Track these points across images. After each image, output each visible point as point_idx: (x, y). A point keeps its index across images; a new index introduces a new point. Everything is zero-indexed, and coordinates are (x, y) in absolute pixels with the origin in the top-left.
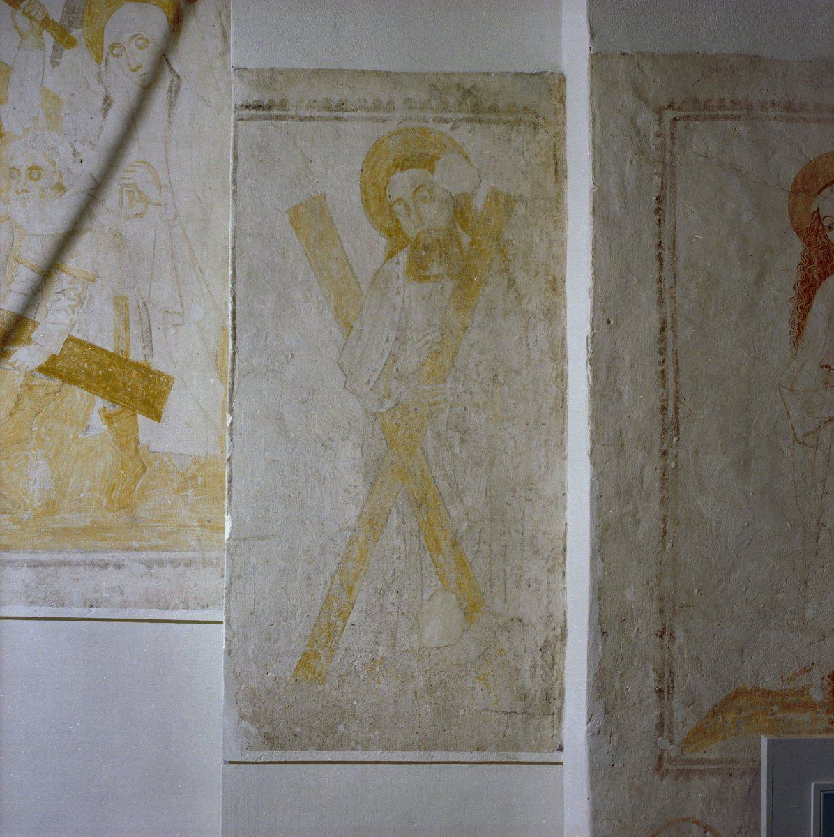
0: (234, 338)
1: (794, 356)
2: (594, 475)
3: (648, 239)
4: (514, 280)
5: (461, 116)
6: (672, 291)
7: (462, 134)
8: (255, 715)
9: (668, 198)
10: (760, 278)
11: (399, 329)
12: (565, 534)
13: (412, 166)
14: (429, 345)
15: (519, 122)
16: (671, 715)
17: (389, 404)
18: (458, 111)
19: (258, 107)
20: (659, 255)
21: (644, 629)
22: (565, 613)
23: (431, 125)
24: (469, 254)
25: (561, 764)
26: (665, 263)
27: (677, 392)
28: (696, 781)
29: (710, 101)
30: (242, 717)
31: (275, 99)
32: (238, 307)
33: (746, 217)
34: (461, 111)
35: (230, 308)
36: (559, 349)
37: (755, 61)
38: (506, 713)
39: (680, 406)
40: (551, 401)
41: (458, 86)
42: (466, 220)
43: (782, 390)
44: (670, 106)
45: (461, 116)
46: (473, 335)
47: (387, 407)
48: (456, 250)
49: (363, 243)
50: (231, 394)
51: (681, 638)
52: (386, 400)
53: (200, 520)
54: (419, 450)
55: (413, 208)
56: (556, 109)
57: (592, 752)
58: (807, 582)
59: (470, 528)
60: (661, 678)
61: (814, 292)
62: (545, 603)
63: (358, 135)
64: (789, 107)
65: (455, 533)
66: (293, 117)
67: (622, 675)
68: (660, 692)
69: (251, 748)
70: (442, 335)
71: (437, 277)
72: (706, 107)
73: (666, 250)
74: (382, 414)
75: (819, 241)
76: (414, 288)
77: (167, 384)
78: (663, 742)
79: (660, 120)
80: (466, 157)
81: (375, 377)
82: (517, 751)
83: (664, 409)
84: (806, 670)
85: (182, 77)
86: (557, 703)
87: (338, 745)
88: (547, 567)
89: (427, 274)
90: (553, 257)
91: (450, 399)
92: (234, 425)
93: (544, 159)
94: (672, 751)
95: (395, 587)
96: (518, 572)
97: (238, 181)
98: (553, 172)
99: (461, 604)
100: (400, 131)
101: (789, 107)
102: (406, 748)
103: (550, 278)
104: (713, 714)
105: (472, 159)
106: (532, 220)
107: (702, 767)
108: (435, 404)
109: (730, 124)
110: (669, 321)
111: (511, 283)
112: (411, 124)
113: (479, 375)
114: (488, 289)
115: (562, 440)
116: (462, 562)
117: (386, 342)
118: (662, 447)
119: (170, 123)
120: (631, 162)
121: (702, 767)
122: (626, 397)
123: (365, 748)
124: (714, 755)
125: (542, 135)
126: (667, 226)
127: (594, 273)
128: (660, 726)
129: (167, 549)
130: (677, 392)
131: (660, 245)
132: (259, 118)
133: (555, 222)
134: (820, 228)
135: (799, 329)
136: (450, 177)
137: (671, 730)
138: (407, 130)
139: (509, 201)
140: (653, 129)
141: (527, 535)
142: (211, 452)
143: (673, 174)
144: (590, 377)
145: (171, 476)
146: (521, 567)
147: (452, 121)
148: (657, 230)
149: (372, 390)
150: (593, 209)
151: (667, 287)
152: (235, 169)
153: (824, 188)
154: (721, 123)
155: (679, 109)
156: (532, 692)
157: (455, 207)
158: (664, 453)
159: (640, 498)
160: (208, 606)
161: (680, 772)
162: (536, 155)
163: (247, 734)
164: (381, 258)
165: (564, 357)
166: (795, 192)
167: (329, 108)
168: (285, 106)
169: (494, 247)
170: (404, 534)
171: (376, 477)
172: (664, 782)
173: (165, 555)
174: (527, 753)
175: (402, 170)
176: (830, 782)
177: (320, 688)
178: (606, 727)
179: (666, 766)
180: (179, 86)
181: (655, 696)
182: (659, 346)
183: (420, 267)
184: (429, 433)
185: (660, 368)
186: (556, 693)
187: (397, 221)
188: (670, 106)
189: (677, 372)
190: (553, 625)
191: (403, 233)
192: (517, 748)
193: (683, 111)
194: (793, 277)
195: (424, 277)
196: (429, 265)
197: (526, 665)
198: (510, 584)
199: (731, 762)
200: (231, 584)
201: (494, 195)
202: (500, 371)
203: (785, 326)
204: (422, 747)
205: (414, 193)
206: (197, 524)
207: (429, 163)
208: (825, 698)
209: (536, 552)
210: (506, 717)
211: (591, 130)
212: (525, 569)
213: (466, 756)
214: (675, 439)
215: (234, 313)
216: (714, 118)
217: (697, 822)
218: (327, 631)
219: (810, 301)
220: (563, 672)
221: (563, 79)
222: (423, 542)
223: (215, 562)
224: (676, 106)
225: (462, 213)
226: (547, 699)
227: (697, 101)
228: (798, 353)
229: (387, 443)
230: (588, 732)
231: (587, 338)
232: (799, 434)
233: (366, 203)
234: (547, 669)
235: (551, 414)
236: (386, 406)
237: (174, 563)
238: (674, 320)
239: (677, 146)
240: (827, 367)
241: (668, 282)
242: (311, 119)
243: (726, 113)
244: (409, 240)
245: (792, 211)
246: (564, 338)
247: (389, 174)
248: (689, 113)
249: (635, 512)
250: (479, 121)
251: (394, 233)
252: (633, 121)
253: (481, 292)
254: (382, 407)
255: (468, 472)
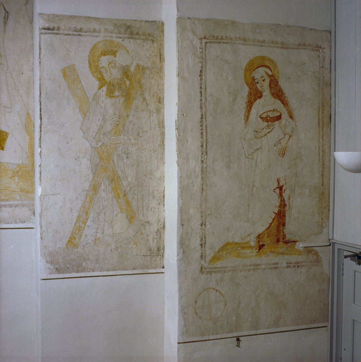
0: (41, 119)
1: (245, 128)
2: (179, 170)
3: (197, 86)
4: (145, 98)
5: (126, 36)
6: (205, 104)
7: (126, 43)
8: (52, 261)
9: (204, 71)
10: (235, 99)
11: (104, 116)
12: (164, 191)
13: (108, 54)
14: (114, 122)
15: (147, 39)
16: (205, 253)
17: (100, 144)
18: (125, 34)
19: (49, 29)
20: (201, 91)
21: (196, 223)
22: (164, 219)
23: (115, 39)
24: (131, 87)
25: (164, 273)
26: (203, 94)
27: (207, 140)
28: (213, 275)
29: (218, 36)
30: (47, 262)
31: (55, 26)
32: (42, 107)
33: (230, 78)
34: (125, 34)
35: (39, 108)
36: (162, 124)
37: (233, 23)
38: (144, 256)
39: (208, 145)
40: (159, 143)
41: (125, 25)
42: (128, 75)
43: (241, 139)
44: (205, 38)
45: (126, 36)
46: (131, 118)
47: (99, 145)
48: (124, 86)
49: (90, 83)
50: (40, 140)
51: (208, 226)
52: (99, 143)
53: (20, 189)
54: (111, 161)
55: (108, 70)
56: (160, 35)
57: (179, 267)
58: (249, 205)
59: (130, 189)
60: (201, 240)
61: (252, 105)
62: (157, 215)
63: (88, 42)
64: (245, 40)
65: (125, 191)
66: (62, 34)
67: (189, 239)
68: (201, 245)
69: (51, 273)
70: (119, 118)
71: (117, 96)
72: (217, 39)
73: (203, 89)
74: (97, 148)
75: (254, 87)
76: (109, 101)
77: (6, 136)
78: (203, 262)
79: (201, 43)
80: (128, 52)
81: (95, 134)
82: (148, 269)
83: (202, 146)
84: (249, 235)
85: (9, 12)
86: (162, 251)
87: (83, 270)
88: (158, 203)
89: (114, 95)
90: (159, 90)
91: (123, 142)
92: (42, 152)
93: (156, 54)
94: (206, 265)
95: (103, 212)
96: (148, 205)
97: (41, 58)
98: (159, 58)
99: (127, 217)
100: (103, 41)
101: (245, 40)
102: (108, 270)
103: (158, 98)
104: (219, 251)
105: (130, 52)
106: (152, 76)
107: (215, 270)
108: (117, 144)
109: (225, 45)
110: (204, 114)
111: (144, 99)
112: (107, 38)
113: (133, 133)
114: (136, 101)
115: (163, 157)
116: (128, 202)
117: (99, 120)
118: (201, 159)
119: (4, 31)
120: (191, 57)
121: (215, 270)
122: (189, 142)
123: (93, 271)
124: (220, 266)
125: (155, 44)
126: (204, 81)
127: (178, 97)
128: (202, 256)
129: (7, 200)
130: (207, 140)
131: (201, 88)
132: (49, 33)
133: (160, 77)
134: (254, 83)
135: (247, 118)
136: (121, 59)
137: (205, 258)
138: (106, 41)
139: (143, 68)
140: (199, 45)
141: (150, 192)
142: (24, 162)
143: (206, 62)
144: (177, 135)
145: (8, 172)
146: (149, 203)
147: (122, 38)
148: (200, 83)
149: (94, 139)
150: (178, 74)
151: (203, 102)
152: (40, 53)
153: (255, 69)
154: (222, 44)
155: (208, 39)
156: (153, 248)
157: (124, 70)
158: (202, 161)
159: (194, 177)
160: (24, 222)
161: (208, 272)
162: (153, 52)
163: (49, 268)
164: (96, 89)
165: (163, 126)
166: (246, 70)
167: (76, 31)
168: (59, 29)
169: (138, 86)
170: (106, 192)
171: (96, 171)
172: (203, 276)
173: (7, 203)
174: (151, 270)
175: (104, 56)
176: (288, 265)
177: (76, 250)
178: (183, 258)
179: (204, 270)
180: (8, 16)
181: (200, 246)
182: (201, 124)
183: (111, 92)
184: (115, 155)
185: (201, 132)
186: (162, 248)
187: (102, 75)
188: (205, 38)
189: (206, 132)
190: (160, 223)
191: (105, 80)
192: (148, 268)
193: (209, 40)
194: (246, 100)
195: (113, 97)
196: (114, 92)
197: (151, 238)
198: (145, 209)
199: (225, 268)
200: (42, 212)
201: (138, 66)
202: (140, 131)
203: (243, 117)
204: (114, 270)
205: (108, 65)
206: (19, 190)
207: (114, 53)
208: (255, 245)
209: (154, 197)
210: (144, 257)
211: (177, 45)
212: (150, 204)
213: (130, 272)
214: (206, 156)
215: (40, 109)
216: (219, 43)
217: (214, 289)
218: (79, 228)
219: (251, 108)
220: (164, 240)
221: (163, 24)
222: (113, 195)
223: (27, 205)
224: (207, 38)
225: (126, 73)
226: (158, 250)
227: (214, 36)
228: (247, 126)
229: (100, 158)
230: (177, 260)
231: (176, 120)
232: (247, 154)
233: (90, 67)
234: (158, 239)
235: (159, 147)
236: (99, 145)
237: (11, 206)
238: (206, 115)
239: (207, 52)
240: (256, 131)
241: (204, 101)
242: (69, 34)
243: (223, 41)
244: (107, 83)
245: (245, 76)
246: (163, 120)
247: (99, 57)
248: (211, 41)
249: (193, 182)
250: (133, 38)
251: (102, 81)
252: (192, 43)
253: (133, 102)
254: (97, 145)
255: (129, 169)
